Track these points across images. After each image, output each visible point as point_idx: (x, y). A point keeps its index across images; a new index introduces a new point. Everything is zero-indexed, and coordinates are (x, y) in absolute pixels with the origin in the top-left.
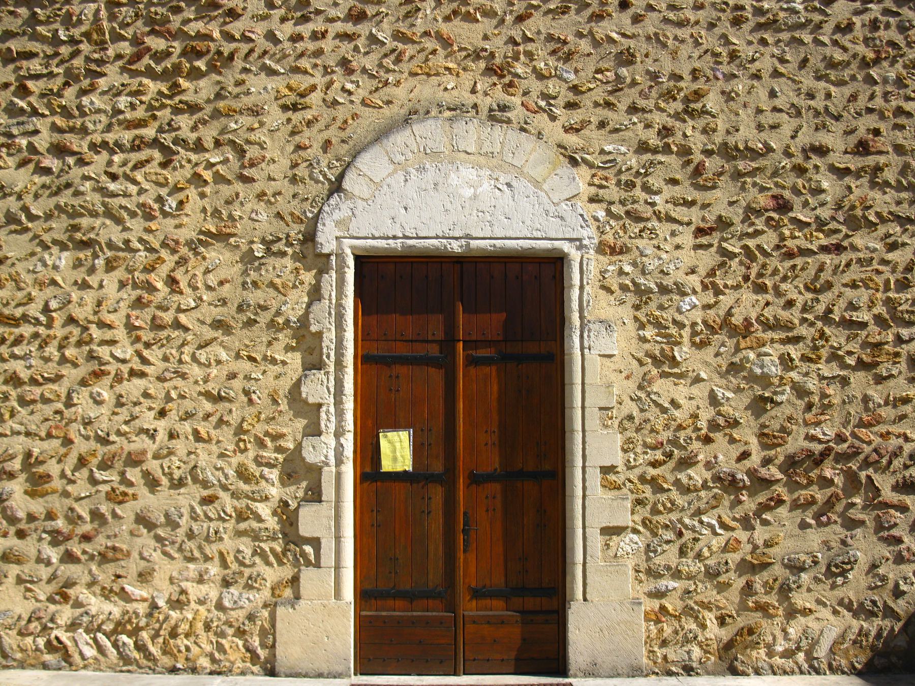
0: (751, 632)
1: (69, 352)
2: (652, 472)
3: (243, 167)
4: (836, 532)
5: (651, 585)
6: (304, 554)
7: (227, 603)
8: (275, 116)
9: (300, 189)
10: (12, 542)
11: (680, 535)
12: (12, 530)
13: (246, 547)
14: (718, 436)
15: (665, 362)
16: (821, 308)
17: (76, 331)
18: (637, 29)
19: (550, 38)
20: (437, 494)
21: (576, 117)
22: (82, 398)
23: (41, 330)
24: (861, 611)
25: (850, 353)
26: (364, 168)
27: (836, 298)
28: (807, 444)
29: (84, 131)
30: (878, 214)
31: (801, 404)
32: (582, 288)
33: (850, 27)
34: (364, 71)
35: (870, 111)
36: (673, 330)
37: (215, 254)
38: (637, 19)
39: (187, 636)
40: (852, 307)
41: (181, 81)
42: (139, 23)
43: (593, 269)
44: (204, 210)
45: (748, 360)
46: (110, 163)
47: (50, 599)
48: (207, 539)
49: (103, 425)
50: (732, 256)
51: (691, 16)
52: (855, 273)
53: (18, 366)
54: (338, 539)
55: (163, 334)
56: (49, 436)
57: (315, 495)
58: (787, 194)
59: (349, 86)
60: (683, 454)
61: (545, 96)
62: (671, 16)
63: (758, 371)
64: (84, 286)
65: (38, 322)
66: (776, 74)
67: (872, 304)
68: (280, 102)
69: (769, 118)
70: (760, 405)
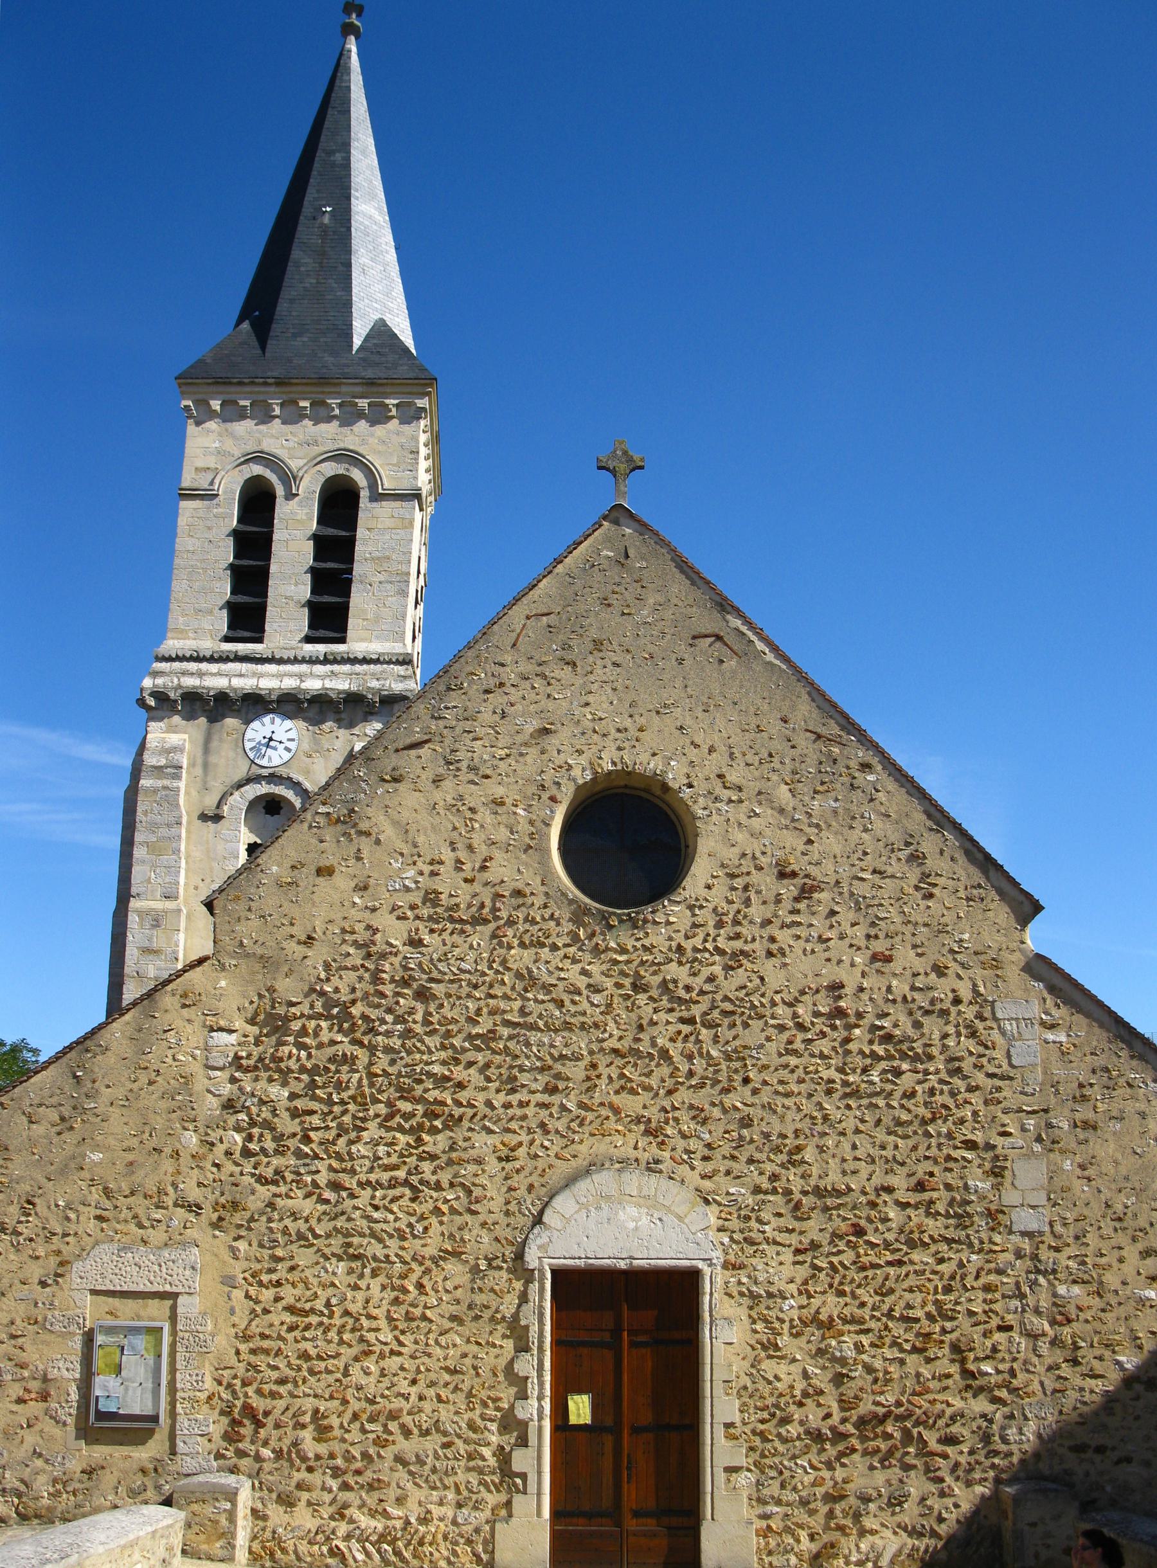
0: (833, 1546)
1: (346, 1337)
2: (761, 1427)
3: (470, 1203)
4: (896, 1472)
5: (760, 1510)
6: (515, 1485)
7: (460, 1520)
8: (493, 1166)
9: (512, 1220)
10: (304, 1475)
11: (781, 1473)
12: (304, 1466)
13: (473, 1478)
14: (808, 1401)
15: (770, 1347)
16: (885, 1308)
17: (351, 1321)
18: (755, 1100)
19: (691, 1107)
20: (608, 1440)
21: (709, 1167)
22: (355, 1370)
23: (325, 1320)
24: (914, 1533)
25: (907, 1341)
26: (558, 1208)
27: (896, 1302)
28: (873, 1408)
29: (353, 1172)
30: (931, 1237)
31: (870, 1378)
32: (711, 1294)
33: (913, 1094)
34: (557, 1132)
35: (927, 1158)
36: (777, 1325)
37: (451, 1266)
38: (755, 1092)
39: (431, 1544)
40: (909, 1306)
41: (424, 1136)
42: (392, 1090)
43: (719, 1280)
44: (443, 1234)
45: (830, 1345)
46: (373, 1197)
47: (332, 1518)
48: (446, 1473)
49: (371, 1391)
50: (820, 1269)
51: (795, 1088)
52: (912, 1281)
53: (308, 1346)
54: (540, 1473)
55: (414, 1324)
56: (332, 1397)
57: (523, 1442)
58: (863, 1223)
59: (546, 1143)
60: (783, 1414)
61: (687, 1152)
62: (780, 1089)
63: (838, 1354)
64: (356, 1287)
65: (322, 1314)
66: (857, 1131)
67: (924, 1304)
69: (850, 1166)
70: (839, 1379)
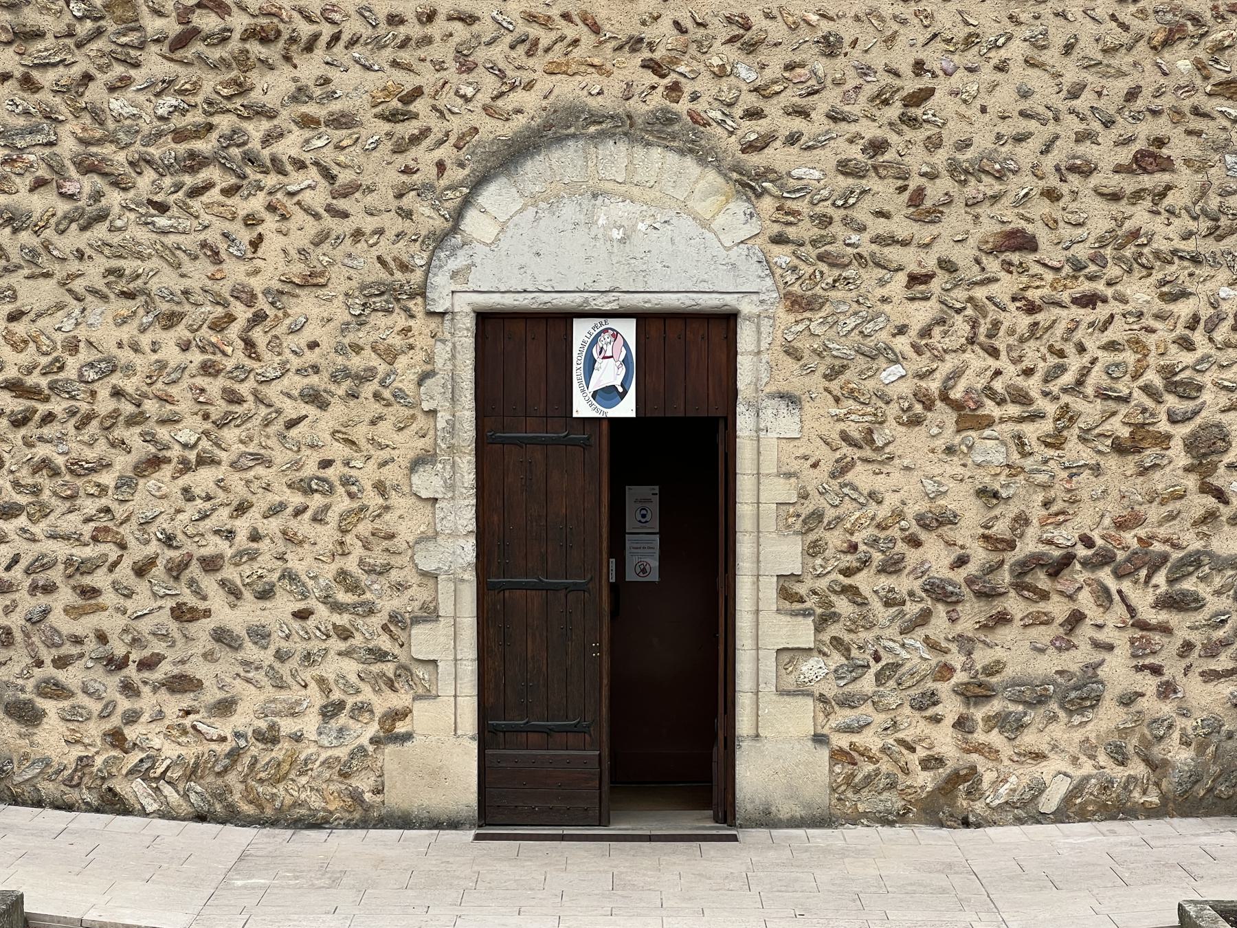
68: (378, 110)
